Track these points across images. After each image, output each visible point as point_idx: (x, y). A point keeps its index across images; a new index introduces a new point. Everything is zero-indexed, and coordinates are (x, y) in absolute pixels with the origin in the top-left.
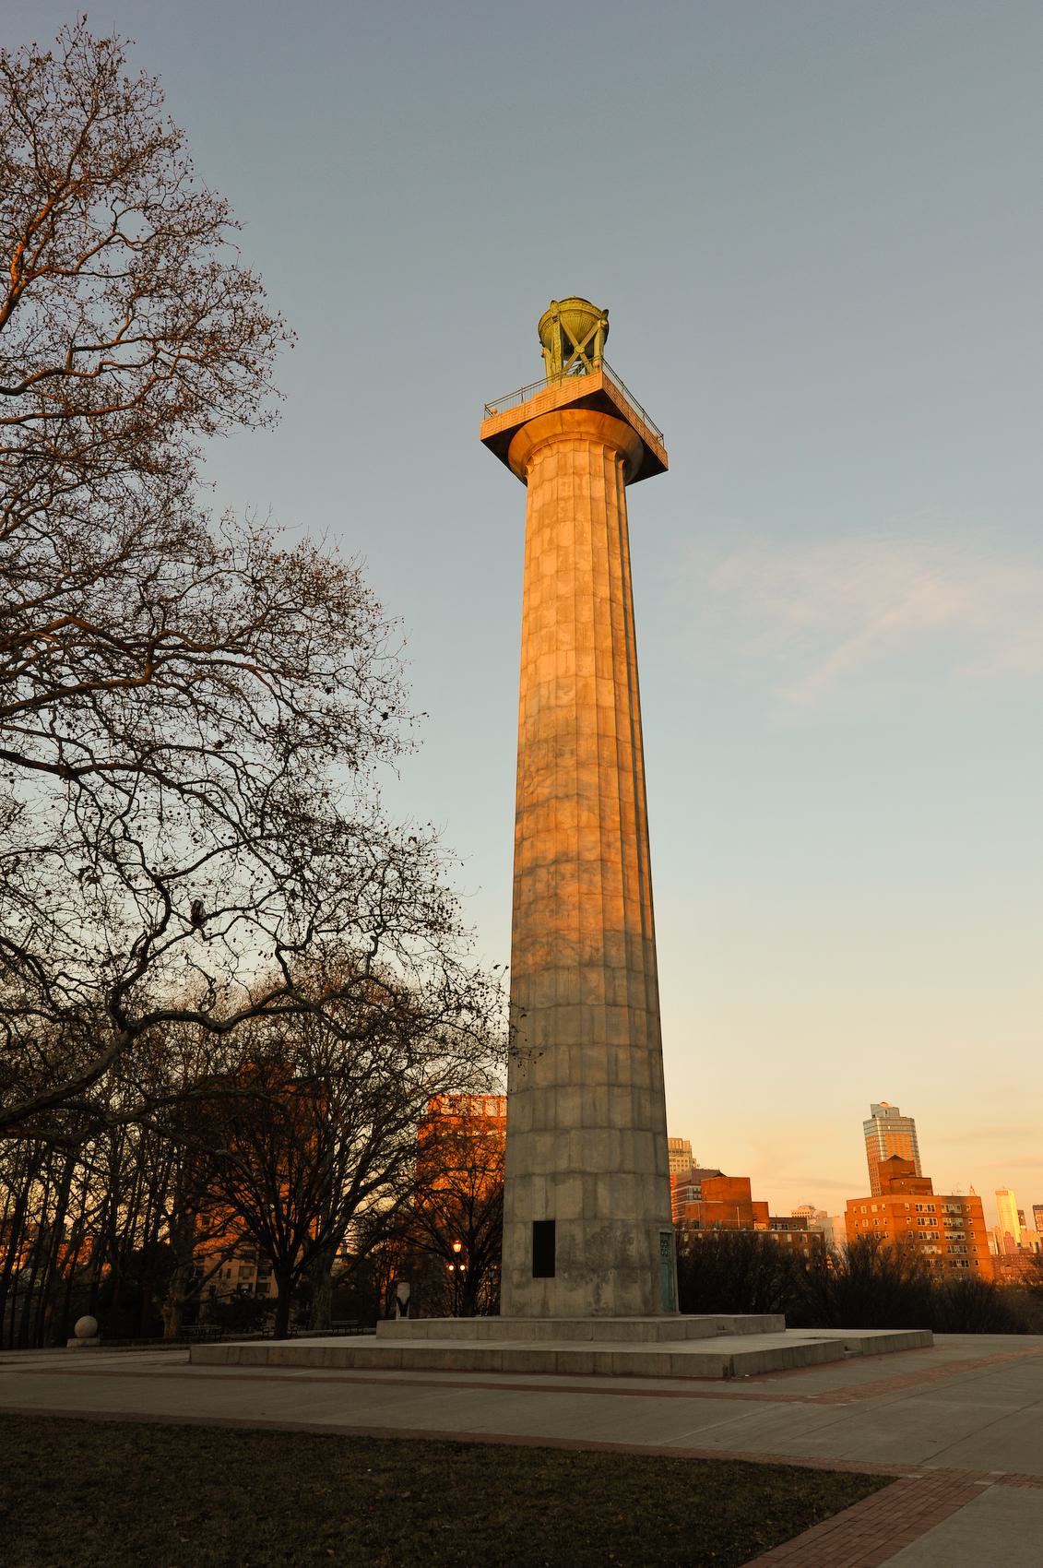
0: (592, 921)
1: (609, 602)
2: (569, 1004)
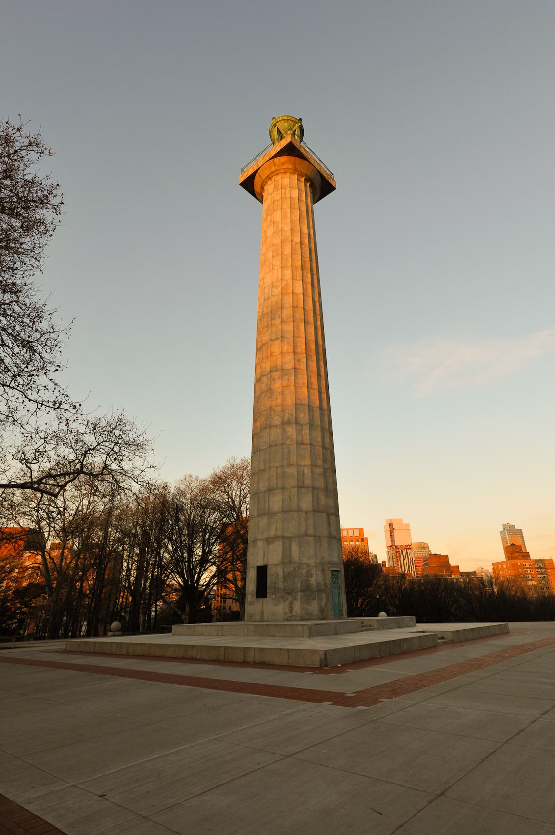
0: (289, 400)
1: (300, 244)
2: (277, 445)
